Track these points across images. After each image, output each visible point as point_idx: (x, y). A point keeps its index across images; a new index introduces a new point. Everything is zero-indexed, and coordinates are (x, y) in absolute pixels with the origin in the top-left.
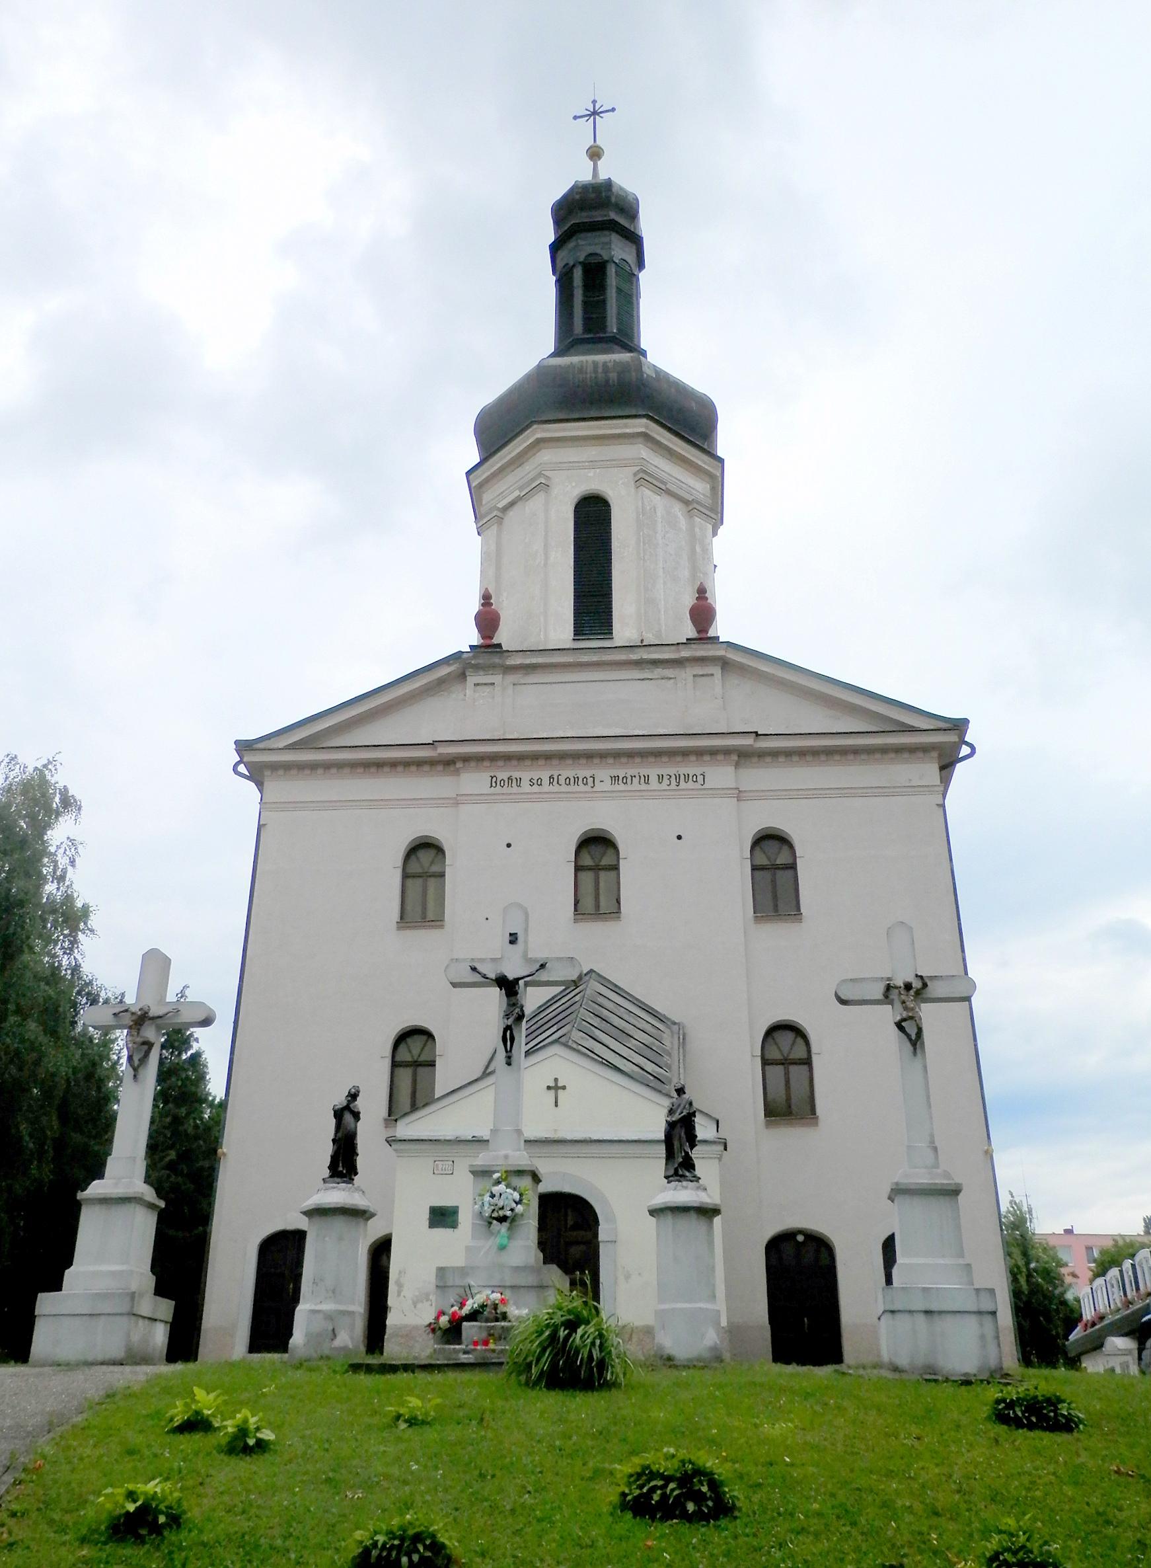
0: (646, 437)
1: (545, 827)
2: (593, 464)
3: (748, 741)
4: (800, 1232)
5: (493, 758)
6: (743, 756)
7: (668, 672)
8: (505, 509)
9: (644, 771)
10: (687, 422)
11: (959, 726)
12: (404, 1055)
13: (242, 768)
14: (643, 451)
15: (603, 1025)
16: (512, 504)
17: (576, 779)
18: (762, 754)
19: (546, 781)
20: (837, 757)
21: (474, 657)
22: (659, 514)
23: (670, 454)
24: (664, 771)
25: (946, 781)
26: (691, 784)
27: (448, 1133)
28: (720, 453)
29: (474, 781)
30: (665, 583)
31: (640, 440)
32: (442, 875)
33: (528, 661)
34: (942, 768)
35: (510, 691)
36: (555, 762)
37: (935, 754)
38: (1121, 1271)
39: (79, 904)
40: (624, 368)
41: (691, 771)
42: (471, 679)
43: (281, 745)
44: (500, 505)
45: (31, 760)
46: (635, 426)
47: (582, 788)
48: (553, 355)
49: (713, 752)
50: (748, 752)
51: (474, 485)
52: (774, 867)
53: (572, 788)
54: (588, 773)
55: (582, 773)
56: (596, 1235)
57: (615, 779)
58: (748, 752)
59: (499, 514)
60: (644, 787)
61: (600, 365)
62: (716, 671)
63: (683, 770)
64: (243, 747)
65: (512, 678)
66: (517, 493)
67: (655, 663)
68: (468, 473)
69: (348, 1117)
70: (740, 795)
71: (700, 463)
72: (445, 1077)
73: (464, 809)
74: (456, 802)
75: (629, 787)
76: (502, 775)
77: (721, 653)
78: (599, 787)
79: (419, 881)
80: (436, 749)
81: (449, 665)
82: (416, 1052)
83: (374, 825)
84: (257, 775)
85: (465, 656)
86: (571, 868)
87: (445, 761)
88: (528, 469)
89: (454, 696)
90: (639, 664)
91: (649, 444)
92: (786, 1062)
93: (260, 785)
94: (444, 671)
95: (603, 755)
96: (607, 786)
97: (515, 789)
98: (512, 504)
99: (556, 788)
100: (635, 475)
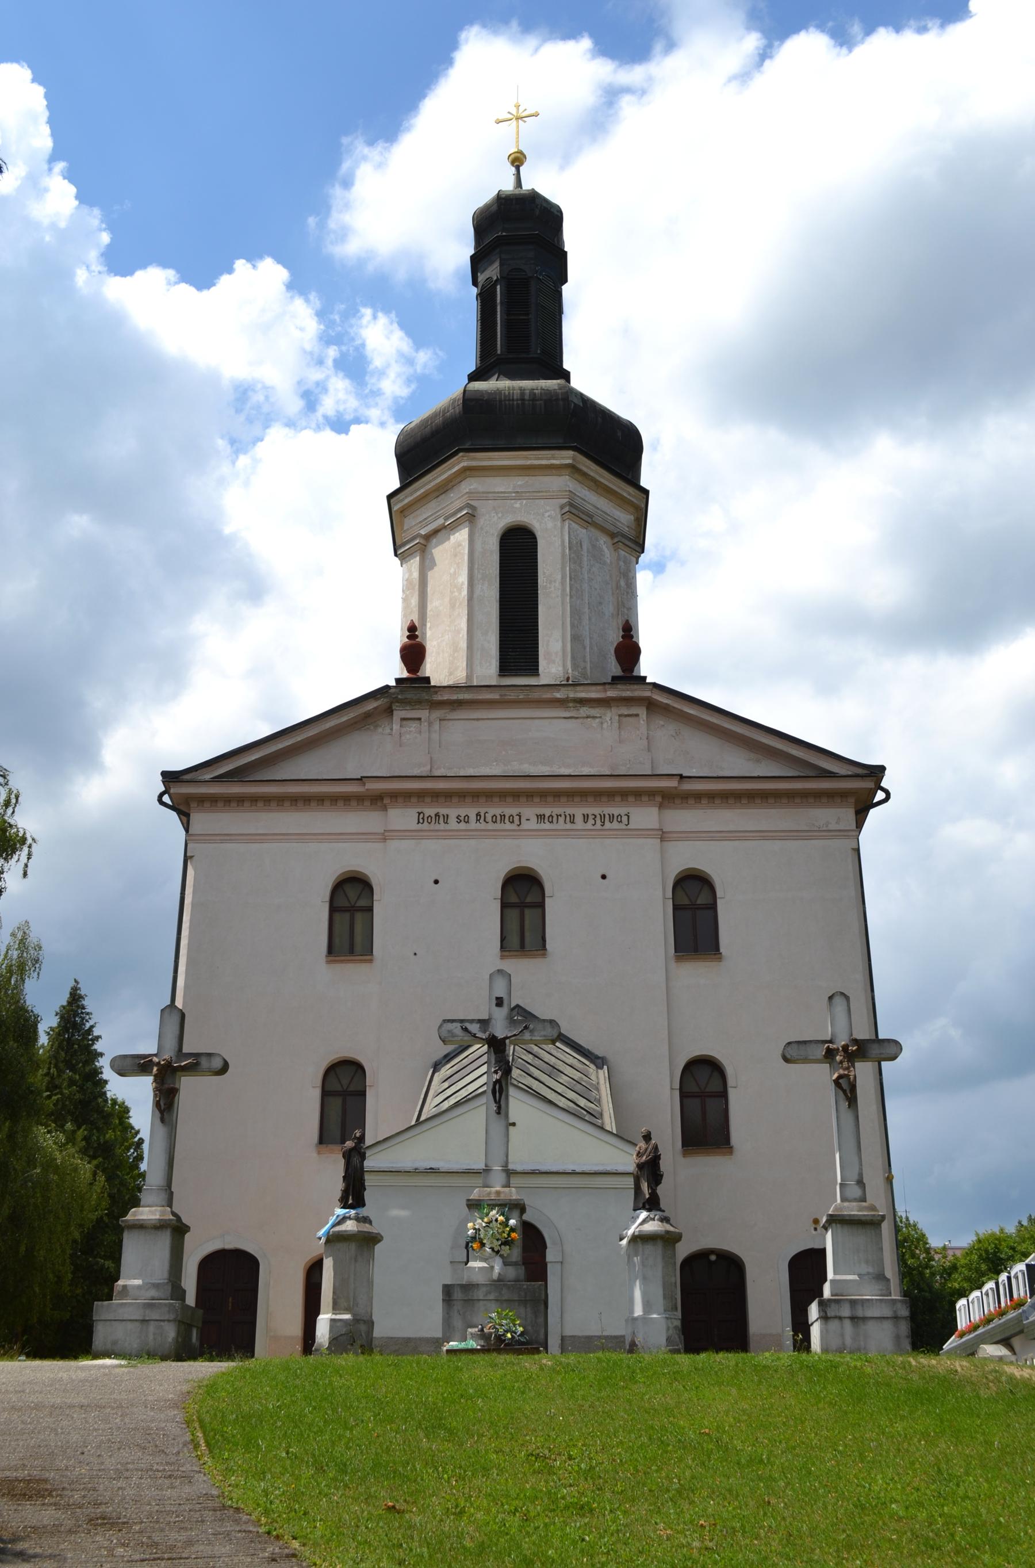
0: (574, 469)
2: (519, 495)
3: (673, 783)
4: (712, 1251)
6: (667, 799)
8: (428, 537)
10: (611, 446)
11: (878, 772)
13: (166, 799)
14: (562, 483)
15: (537, 1062)
17: (503, 816)
19: (473, 818)
21: (402, 692)
22: (585, 547)
25: (860, 824)
26: (615, 825)
27: (408, 1164)
28: (643, 483)
29: (402, 817)
30: (590, 619)
31: (568, 471)
32: (370, 909)
33: (455, 697)
35: (436, 726)
36: (482, 800)
37: (852, 800)
38: (997, 1284)
40: (550, 399)
41: (616, 811)
42: (399, 714)
43: (208, 777)
44: (423, 532)
46: (563, 458)
47: (508, 826)
48: (473, 377)
50: (675, 794)
51: (395, 508)
52: (695, 918)
53: (499, 826)
54: (514, 811)
55: (509, 811)
56: (544, 1256)
57: (541, 817)
58: (675, 794)
59: (422, 541)
60: (569, 826)
62: (642, 712)
64: (170, 778)
65: (437, 714)
66: (441, 521)
67: (582, 702)
69: (356, 1160)
70: (663, 836)
71: (625, 494)
73: (393, 844)
74: (384, 837)
76: (430, 811)
77: (647, 694)
78: (525, 825)
79: (347, 916)
80: (364, 785)
81: (377, 699)
82: (345, 1082)
83: (299, 858)
84: (182, 809)
85: (392, 691)
86: (497, 906)
87: (375, 796)
88: (455, 501)
89: (380, 730)
90: (562, 703)
91: (576, 476)
92: (703, 1096)
93: (184, 815)
94: (371, 705)
96: (533, 824)
97: (442, 826)
98: (436, 532)
99: (482, 825)
100: (562, 507)
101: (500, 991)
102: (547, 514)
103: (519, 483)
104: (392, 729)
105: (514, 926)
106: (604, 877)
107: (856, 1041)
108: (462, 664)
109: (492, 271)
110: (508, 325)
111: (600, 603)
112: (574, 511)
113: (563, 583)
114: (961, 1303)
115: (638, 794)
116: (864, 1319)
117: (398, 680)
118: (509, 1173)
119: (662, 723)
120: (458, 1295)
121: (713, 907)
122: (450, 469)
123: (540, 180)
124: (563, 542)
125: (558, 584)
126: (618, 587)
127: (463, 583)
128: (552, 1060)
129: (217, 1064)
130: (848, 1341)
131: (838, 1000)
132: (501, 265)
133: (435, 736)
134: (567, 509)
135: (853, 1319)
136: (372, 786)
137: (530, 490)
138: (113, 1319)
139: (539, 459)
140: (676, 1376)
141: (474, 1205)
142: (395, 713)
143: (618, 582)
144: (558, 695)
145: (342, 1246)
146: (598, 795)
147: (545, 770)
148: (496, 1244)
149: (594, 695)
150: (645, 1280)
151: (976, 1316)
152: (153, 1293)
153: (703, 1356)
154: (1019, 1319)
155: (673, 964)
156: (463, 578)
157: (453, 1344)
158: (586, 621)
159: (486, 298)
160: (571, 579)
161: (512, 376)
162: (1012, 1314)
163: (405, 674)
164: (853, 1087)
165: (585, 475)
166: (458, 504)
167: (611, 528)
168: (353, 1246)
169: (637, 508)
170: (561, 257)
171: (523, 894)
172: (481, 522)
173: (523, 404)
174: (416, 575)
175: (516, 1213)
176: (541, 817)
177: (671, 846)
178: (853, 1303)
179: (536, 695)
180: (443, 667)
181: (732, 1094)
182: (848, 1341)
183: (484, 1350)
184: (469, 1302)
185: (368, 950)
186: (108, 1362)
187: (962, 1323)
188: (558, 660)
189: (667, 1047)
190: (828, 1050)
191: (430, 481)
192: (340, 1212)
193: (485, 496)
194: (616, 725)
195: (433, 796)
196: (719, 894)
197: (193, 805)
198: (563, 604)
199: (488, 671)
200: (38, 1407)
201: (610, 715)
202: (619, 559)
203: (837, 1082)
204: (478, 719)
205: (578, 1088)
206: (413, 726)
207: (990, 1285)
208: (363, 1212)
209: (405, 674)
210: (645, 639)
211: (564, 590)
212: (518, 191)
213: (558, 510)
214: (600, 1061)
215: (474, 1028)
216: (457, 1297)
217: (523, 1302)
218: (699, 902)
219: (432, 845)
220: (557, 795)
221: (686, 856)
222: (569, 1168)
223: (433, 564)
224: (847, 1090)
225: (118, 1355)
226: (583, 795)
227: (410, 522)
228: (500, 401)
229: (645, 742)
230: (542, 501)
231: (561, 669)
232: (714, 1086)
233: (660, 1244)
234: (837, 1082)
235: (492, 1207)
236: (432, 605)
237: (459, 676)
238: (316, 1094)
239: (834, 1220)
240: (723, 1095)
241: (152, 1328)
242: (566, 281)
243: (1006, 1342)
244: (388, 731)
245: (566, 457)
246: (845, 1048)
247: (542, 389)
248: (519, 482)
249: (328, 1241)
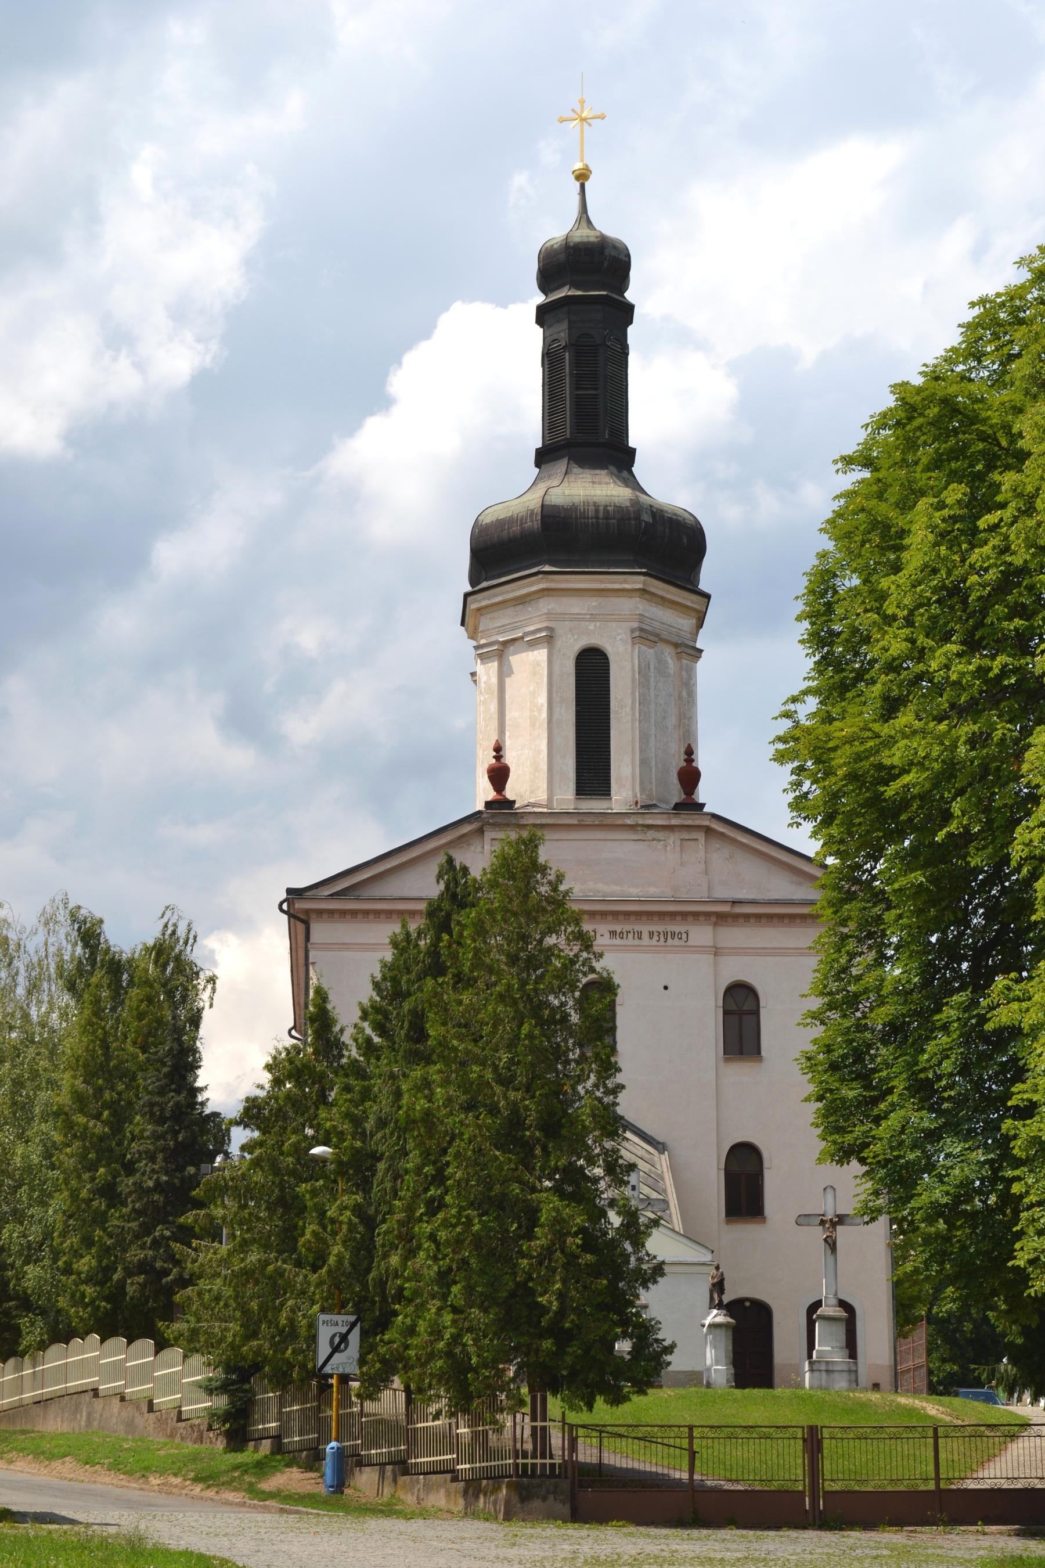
0: (643, 592)
6: (721, 919)
7: (660, 835)
9: (637, 928)
18: (736, 917)
20: (798, 921)
21: (493, 815)
22: (652, 668)
23: (663, 601)
26: (676, 942)
31: (638, 594)
39: (659, 1279)
45: (98, 915)
46: (634, 583)
49: (696, 915)
50: (728, 915)
57: (613, 933)
58: (728, 915)
59: (501, 648)
60: (637, 942)
61: (601, 508)
62: (701, 836)
63: (671, 928)
67: (650, 827)
70: (717, 952)
75: (624, 942)
77: (706, 823)
81: (470, 823)
89: (472, 848)
90: (633, 827)
91: (646, 596)
102: (619, 637)
103: (594, 604)
104: (483, 848)
106: (666, 988)
107: (838, 1216)
108: (544, 785)
111: (665, 718)
112: (644, 635)
113: (633, 708)
119: (718, 846)
122: (528, 586)
123: (608, 224)
124: (633, 666)
125: (628, 709)
126: (680, 697)
127: (542, 705)
130: (824, 1383)
131: (829, 1190)
132: (570, 328)
134: (637, 634)
135: (827, 1371)
137: (608, 611)
139: (612, 583)
140: (735, 1401)
142: (486, 833)
143: (680, 693)
144: (629, 822)
146: (662, 915)
149: (659, 822)
150: (714, 1346)
153: (747, 1391)
155: (722, 1064)
156: (543, 699)
158: (652, 742)
160: (640, 722)
164: (835, 1243)
167: (675, 639)
172: (559, 643)
173: (598, 523)
176: (613, 933)
177: (722, 960)
178: (827, 1363)
182: (824, 1383)
189: (715, 1135)
190: (822, 1221)
191: (508, 592)
193: (561, 617)
194: (678, 849)
196: (761, 1004)
197: (313, 916)
198: (632, 729)
199: (566, 797)
201: (673, 838)
202: (681, 669)
203: (825, 1240)
204: (557, 840)
211: (633, 715)
212: (583, 235)
213: (629, 634)
214: (661, 1146)
218: (745, 1008)
221: (735, 970)
223: (511, 672)
224: (831, 1245)
228: (576, 518)
229: (703, 866)
230: (614, 624)
231: (630, 793)
233: (724, 1329)
234: (825, 1240)
237: (541, 795)
242: (631, 323)
244: (479, 849)
245: (637, 582)
246: (831, 1220)
247: (615, 506)
248: (594, 602)
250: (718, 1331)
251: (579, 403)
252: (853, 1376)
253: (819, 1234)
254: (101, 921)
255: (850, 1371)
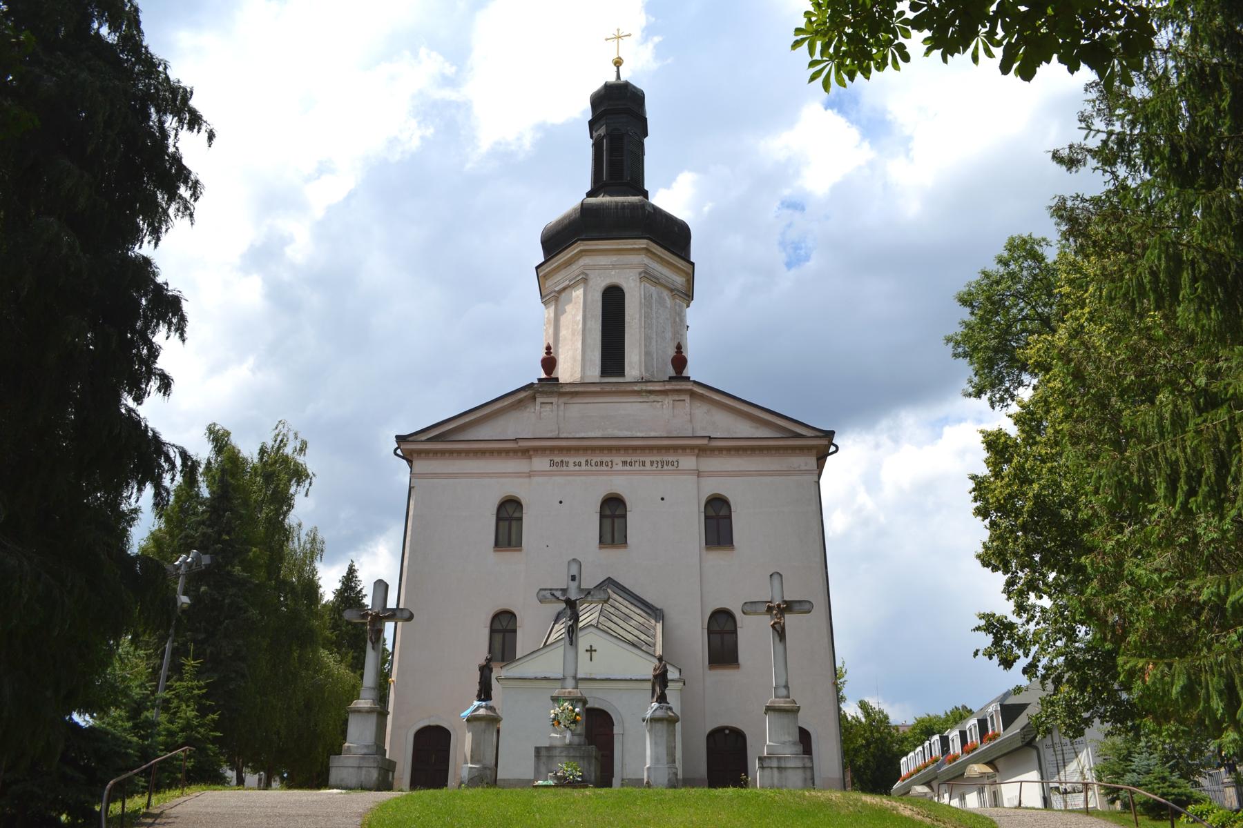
0: (647, 250)
1: (583, 489)
2: (614, 267)
3: (705, 442)
4: (727, 728)
5: (552, 449)
9: (642, 459)
10: (672, 236)
12: (498, 626)
13: (399, 452)
14: (643, 259)
15: (617, 612)
16: (564, 289)
24: (654, 459)
25: (820, 467)
26: (670, 467)
29: (541, 463)
32: (521, 519)
34: (818, 459)
35: (562, 407)
40: (633, 207)
41: (670, 459)
42: (539, 400)
47: (605, 468)
48: (589, 195)
50: (706, 448)
52: (718, 523)
53: (599, 468)
54: (608, 459)
55: (605, 459)
57: (625, 463)
58: (706, 448)
62: (687, 398)
63: (666, 458)
64: (400, 439)
65: (563, 400)
67: (651, 392)
68: (537, 268)
69: (487, 671)
70: (699, 474)
72: (523, 643)
73: (535, 479)
74: (530, 475)
76: (557, 459)
78: (615, 467)
82: (504, 624)
83: (479, 487)
84: (409, 458)
87: (524, 450)
88: (575, 269)
90: (639, 393)
92: (722, 633)
93: (410, 462)
94: (522, 395)
95: (618, 449)
96: (620, 467)
97: (565, 468)
98: (564, 289)
99: (589, 468)
101: (574, 571)
105: (608, 528)
107: (785, 602)
109: (602, 131)
110: (610, 163)
114: (904, 760)
115: (683, 449)
116: (786, 768)
117: (540, 380)
118: (577, 680)
120: (543, 753)
121: (729, 517)
128: (627, 611)
129: (406, 615)
130: (776, 781)
131: (776, 580)
133: (561, 413)
136: (521, 444)
137: (623, 264)
138: (342, 767)
141: (555, 699)
145: (477, 723)
147: (628, 434)
148: (567, 723)
151: (912, 768)
152: (365, 751)
154: (935, 770)
155: (704, 552)
156: (580, 317)
157: (540, 782)
158: (654, 343)
159: (597, 147)
161: (611, 195)
162: (931, 767)
163: (543, 376)
164: (783, 629)
165: (672, 265)
166: (577, 272)
168: (483, 724)
169: (687, 274)
170: (644, 121)
171: (613, 509)
172: (591, 283)
174: (552, 315)
175: (580, 704)
176: (625, 463)
177: (702, 479)
178: (779, 759)
179: (623, 388)
180: (567, 372)
181: (739, 631)
182: (776, 781)
183: (556, 786)
184: (550, 757)
185: (519, 544)
186: (335, 791)
187: (904, 772)
188: (637, 367)
192: (476, 703)
193: (594, 267)
195: (559, 450)
199: (594, 373)
200: (280, 815)
201: (668, 401)
203: (773, 626)
205: (642, 628)
206: (548, 407)
207: (920, 748)
208: (490, 703)
209: (543, 376)
210: (690, 354)
215: (558, 594)
216: (542, 754)
217: (582, 758)
219: (559, 480)
220: (635, 449)
221: (712, 486)
222: (628, 677)
224: (780, 632)
225: (343, 788)
226: (651, 449)
227: (549, 283)
232: (729, 627)
234: (773, 626)
235: (565, 700)
236: (564, 333)
238: (487, 631)
239: (769, 709)
240: (735, 632)
241: (364, 771)
243: (928, 784)
245: (643, 243)
246: (779, 606)
248: (614, 259)
249: (468, 720)
250: (658, 726)
251: (611, 163)
252: (809, 773)
253: (767, 621)
254: (229, 434)
255: (804, 768)
